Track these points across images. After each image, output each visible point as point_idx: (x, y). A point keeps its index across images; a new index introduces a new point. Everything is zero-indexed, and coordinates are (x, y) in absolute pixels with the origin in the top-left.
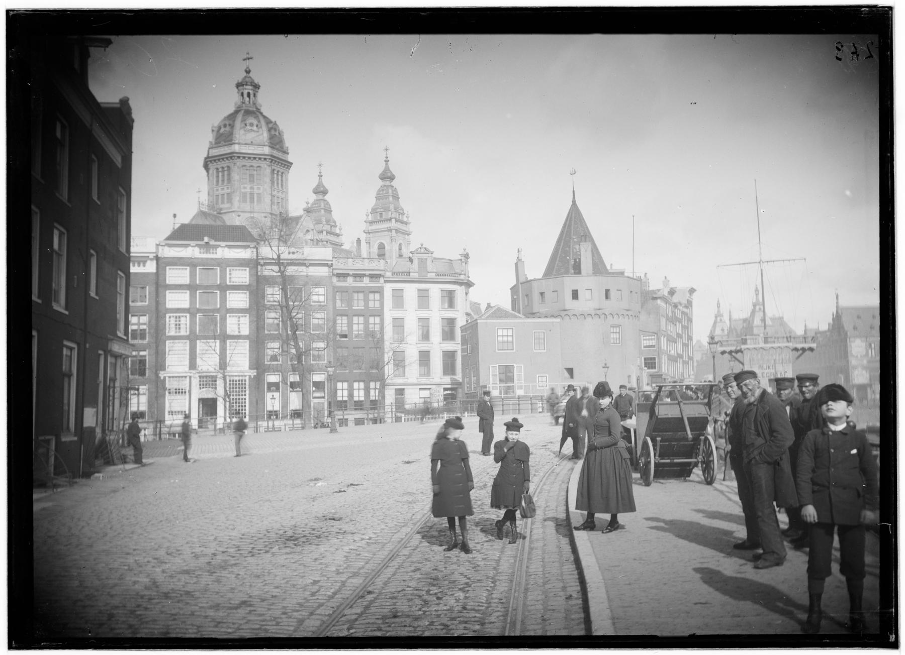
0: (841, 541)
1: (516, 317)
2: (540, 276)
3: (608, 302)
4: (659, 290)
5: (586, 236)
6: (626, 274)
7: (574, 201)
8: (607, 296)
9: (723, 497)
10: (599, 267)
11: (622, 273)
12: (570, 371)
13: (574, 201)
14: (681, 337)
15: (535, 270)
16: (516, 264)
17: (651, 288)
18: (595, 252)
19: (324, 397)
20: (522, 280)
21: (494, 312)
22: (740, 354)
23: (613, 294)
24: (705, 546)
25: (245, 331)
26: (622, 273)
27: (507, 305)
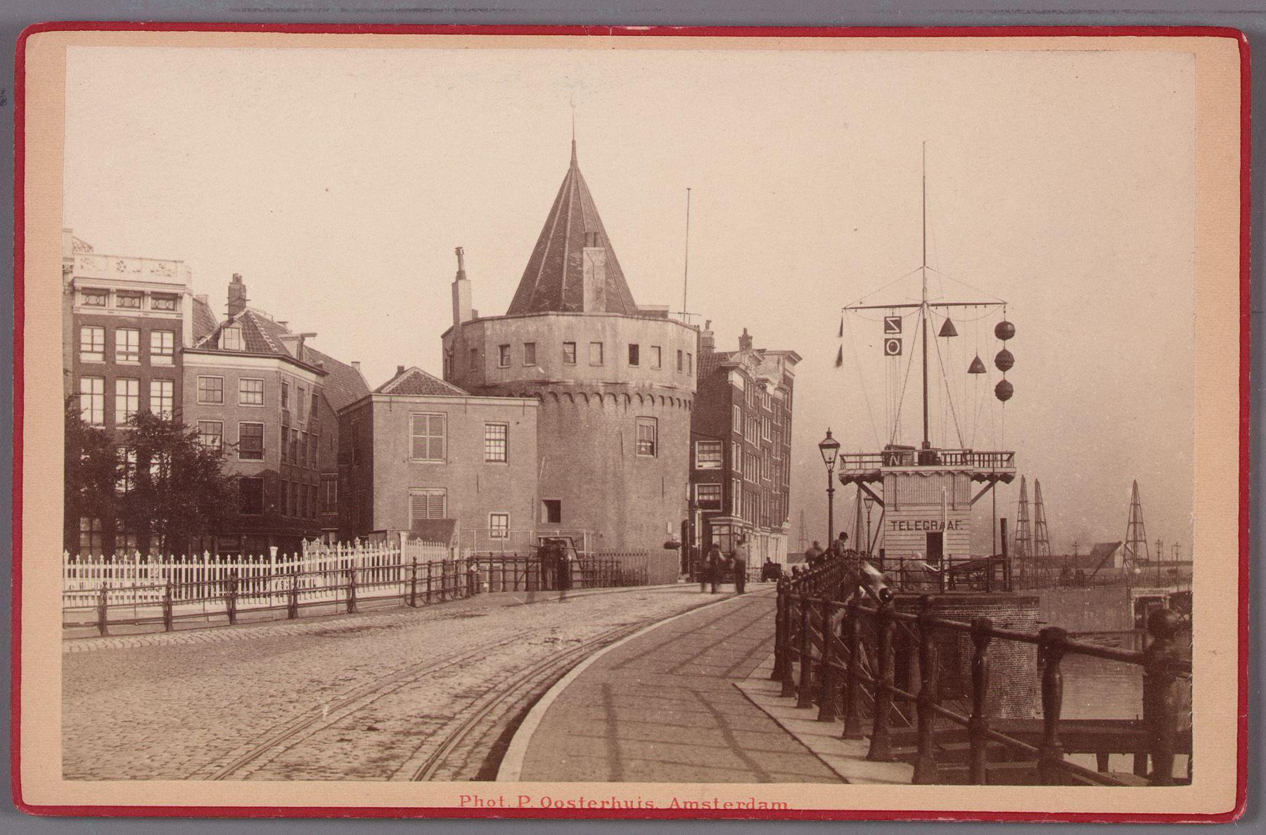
0: (1154, 765)
1: (450, 392)
2: (503, 311)
3: (634, 370)
4: (732, 354)
5: (596, 237)
6: (670, 316)
7: (574, 162)
8: (634, 359)
9: (818, 762)
10: (619, 301)
11: (664, 314)
12: (555, 510)
13: (574, 162)
14: (770, 451)
15: (493, 294)
16: (455, 285)
17: (715, 351)
18: (612, 266)
19: (304, 515)
20: (465, 317)
21: (408, 381)
22: (877, 484)
23: (644, 353)
24: (943, 783)
25: (89, 381)
26: (664, 314)
27: (435, 370)
